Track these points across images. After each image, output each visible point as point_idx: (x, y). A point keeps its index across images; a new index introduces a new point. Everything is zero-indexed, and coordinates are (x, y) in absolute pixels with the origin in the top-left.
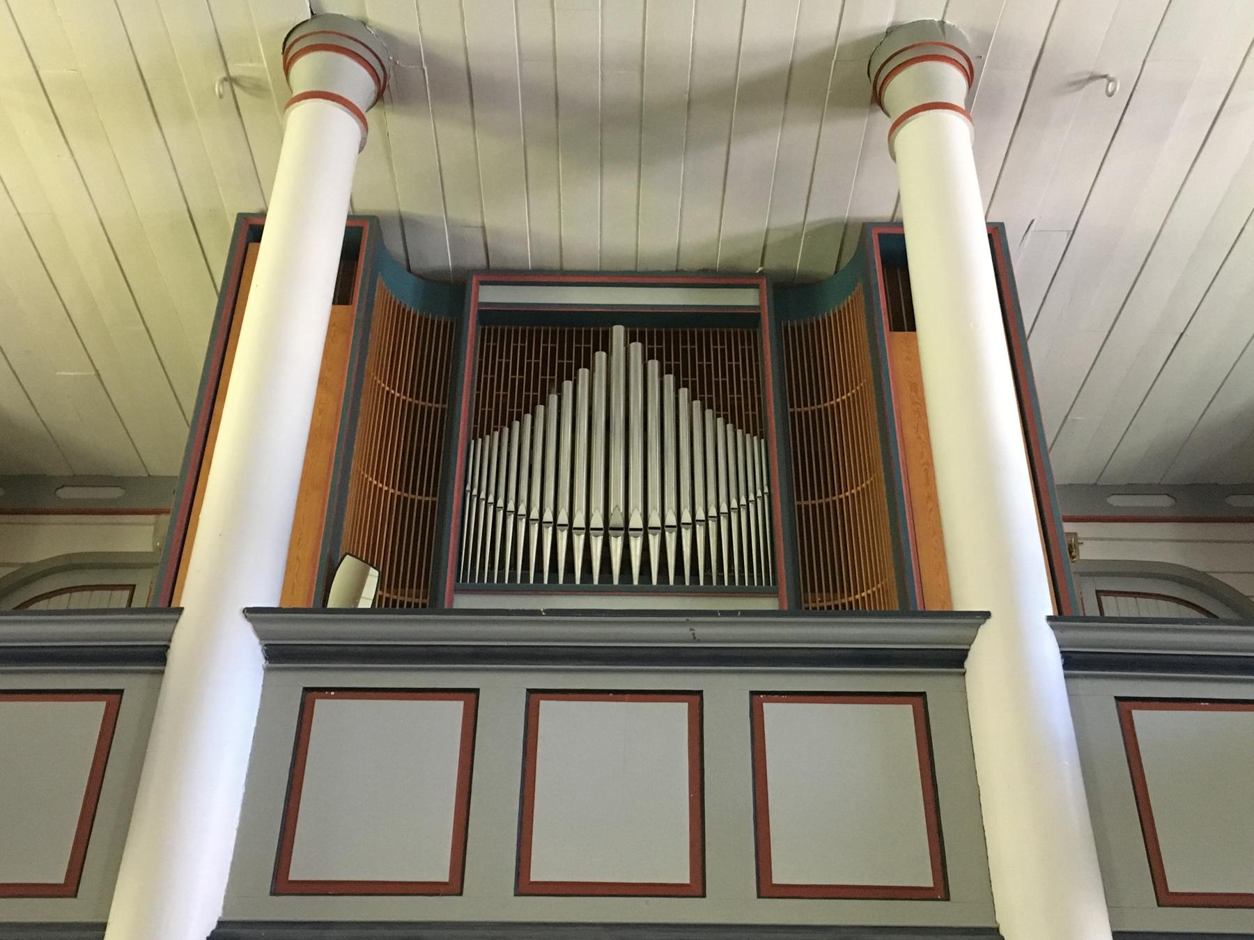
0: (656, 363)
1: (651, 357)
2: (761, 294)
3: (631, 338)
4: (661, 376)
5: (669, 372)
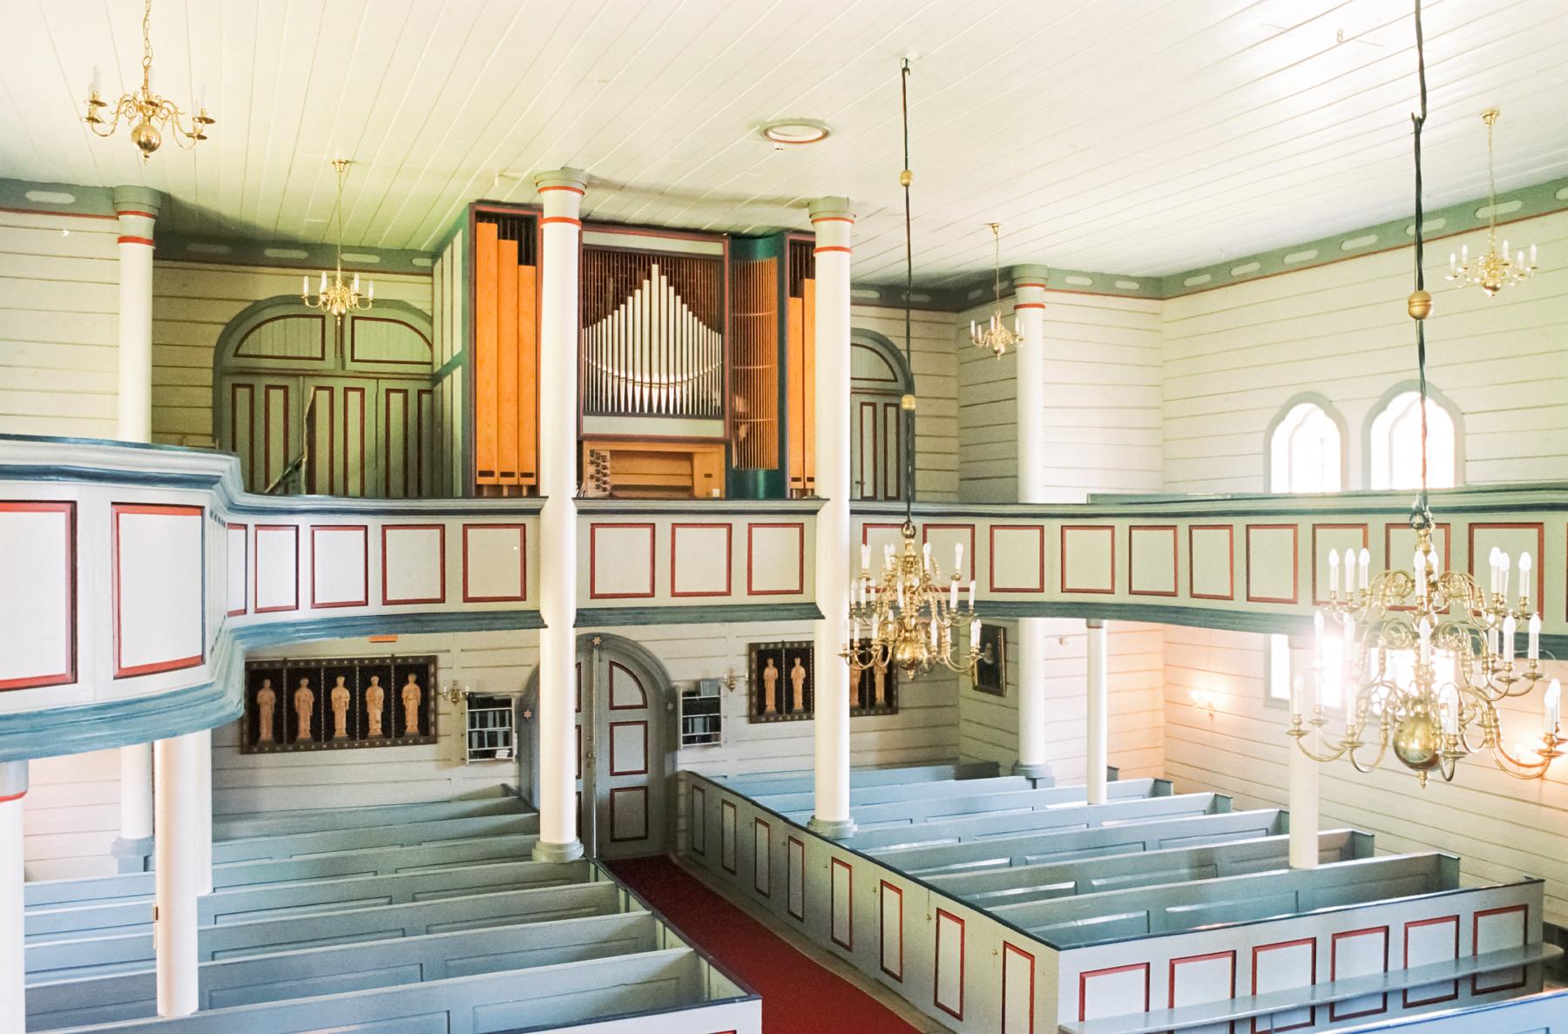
3: (661, 272)
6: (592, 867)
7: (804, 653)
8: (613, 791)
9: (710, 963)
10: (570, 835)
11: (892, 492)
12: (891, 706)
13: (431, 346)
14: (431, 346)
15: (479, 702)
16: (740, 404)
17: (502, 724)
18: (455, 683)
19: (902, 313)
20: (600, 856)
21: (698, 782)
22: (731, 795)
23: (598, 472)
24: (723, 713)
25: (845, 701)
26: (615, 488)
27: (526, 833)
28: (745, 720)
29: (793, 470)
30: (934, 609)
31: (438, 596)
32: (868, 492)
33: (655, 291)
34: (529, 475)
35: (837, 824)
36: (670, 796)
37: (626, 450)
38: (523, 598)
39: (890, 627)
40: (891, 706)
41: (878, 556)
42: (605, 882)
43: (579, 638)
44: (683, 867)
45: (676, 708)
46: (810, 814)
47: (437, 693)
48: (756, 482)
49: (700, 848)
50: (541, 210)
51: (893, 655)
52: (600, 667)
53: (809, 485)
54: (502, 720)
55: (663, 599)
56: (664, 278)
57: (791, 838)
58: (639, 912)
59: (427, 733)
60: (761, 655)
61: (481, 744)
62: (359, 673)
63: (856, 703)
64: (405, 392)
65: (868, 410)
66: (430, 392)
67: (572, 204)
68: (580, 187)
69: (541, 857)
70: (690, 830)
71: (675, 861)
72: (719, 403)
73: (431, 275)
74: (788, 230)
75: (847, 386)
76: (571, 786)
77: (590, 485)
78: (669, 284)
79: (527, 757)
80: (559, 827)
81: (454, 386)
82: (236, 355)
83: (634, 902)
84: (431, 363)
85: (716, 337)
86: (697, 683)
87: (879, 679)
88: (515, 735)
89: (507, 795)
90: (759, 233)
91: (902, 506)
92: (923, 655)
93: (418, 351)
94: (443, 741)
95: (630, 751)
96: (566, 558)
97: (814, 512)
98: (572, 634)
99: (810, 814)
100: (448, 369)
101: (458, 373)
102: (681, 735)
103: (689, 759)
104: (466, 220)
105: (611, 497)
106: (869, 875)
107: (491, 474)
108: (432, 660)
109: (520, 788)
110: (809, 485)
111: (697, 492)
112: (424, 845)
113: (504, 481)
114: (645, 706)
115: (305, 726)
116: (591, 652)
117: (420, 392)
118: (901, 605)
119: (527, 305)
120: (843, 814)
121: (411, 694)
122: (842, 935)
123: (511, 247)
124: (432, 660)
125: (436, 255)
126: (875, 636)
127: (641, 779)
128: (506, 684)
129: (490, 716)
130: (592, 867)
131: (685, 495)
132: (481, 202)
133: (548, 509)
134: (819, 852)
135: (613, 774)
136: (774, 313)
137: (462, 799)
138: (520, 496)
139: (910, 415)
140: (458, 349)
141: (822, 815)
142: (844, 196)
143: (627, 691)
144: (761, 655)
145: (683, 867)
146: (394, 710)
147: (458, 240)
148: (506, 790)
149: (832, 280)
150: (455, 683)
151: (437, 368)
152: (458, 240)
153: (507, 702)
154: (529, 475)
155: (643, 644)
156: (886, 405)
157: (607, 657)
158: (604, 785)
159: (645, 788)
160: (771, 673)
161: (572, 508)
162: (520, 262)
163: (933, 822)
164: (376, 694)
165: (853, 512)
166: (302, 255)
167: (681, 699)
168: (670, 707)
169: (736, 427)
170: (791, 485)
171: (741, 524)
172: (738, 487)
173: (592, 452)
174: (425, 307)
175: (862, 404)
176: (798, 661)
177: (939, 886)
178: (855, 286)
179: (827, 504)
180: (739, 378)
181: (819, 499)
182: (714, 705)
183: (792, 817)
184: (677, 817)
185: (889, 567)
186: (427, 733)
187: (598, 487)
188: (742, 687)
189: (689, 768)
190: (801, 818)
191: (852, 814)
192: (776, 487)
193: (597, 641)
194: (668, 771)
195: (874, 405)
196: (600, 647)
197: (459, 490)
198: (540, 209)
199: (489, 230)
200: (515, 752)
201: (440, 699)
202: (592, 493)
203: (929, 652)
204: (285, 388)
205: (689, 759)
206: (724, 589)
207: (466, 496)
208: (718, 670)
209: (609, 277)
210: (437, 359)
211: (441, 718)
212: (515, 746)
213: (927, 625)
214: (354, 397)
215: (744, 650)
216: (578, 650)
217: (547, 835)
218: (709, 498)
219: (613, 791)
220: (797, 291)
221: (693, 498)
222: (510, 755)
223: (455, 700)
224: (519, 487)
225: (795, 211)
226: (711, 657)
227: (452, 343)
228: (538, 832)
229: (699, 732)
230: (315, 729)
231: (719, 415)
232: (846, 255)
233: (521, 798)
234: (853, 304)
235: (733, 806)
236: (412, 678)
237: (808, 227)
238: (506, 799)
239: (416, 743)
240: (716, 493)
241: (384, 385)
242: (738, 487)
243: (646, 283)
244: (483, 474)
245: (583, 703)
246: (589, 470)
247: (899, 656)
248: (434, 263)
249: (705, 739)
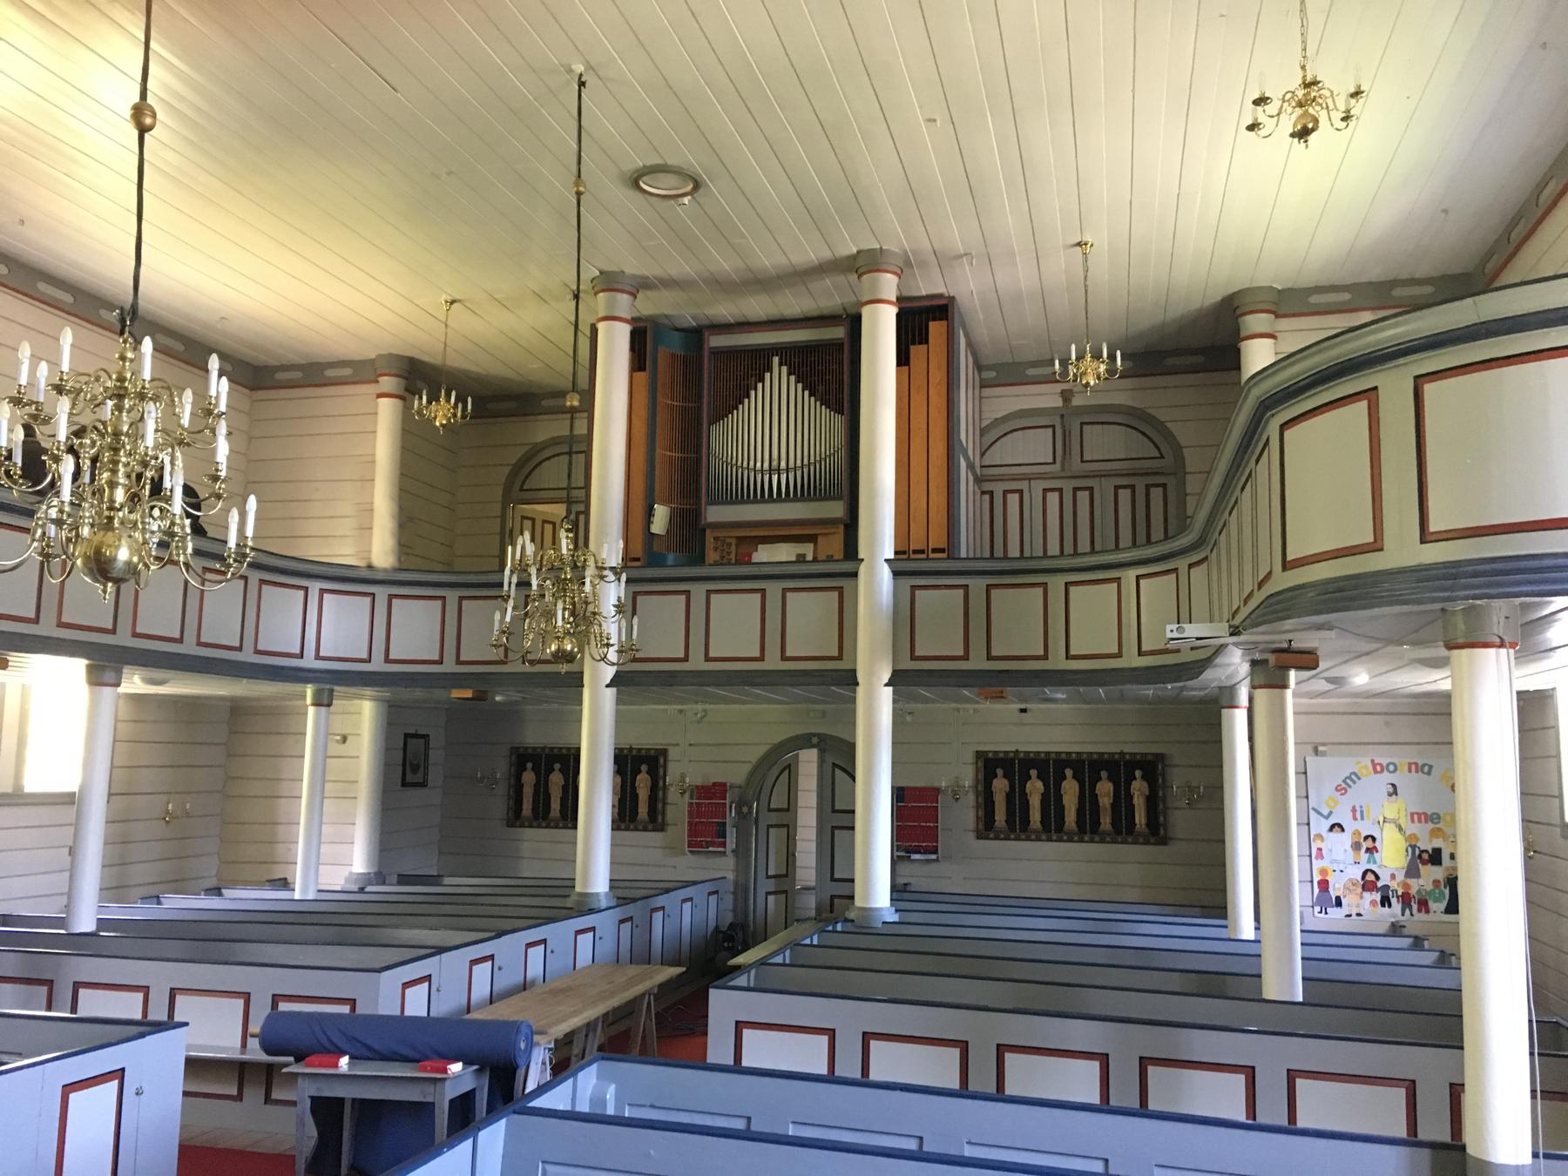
8: (833, 897)
28: (972, 835)
56: (784, 369)
62: (1088, 768)
64: (1060, 490)
78: (797, 382)
82: (521, 490)
94: (670, 829)
115: (1035, 816)
121: (1139, 788)
144: (990, 764)
156: (1076, 489)
160: (1000, 785)
164: (1105, 789)
166: (513, 405)
195: (1132, 488)
204: (1091, 489)
211: (669, 807)
214: (1013, 499)
215: (970, 758)
230: (1010, 821)
236: (644, 768)
241: (1038, 486)
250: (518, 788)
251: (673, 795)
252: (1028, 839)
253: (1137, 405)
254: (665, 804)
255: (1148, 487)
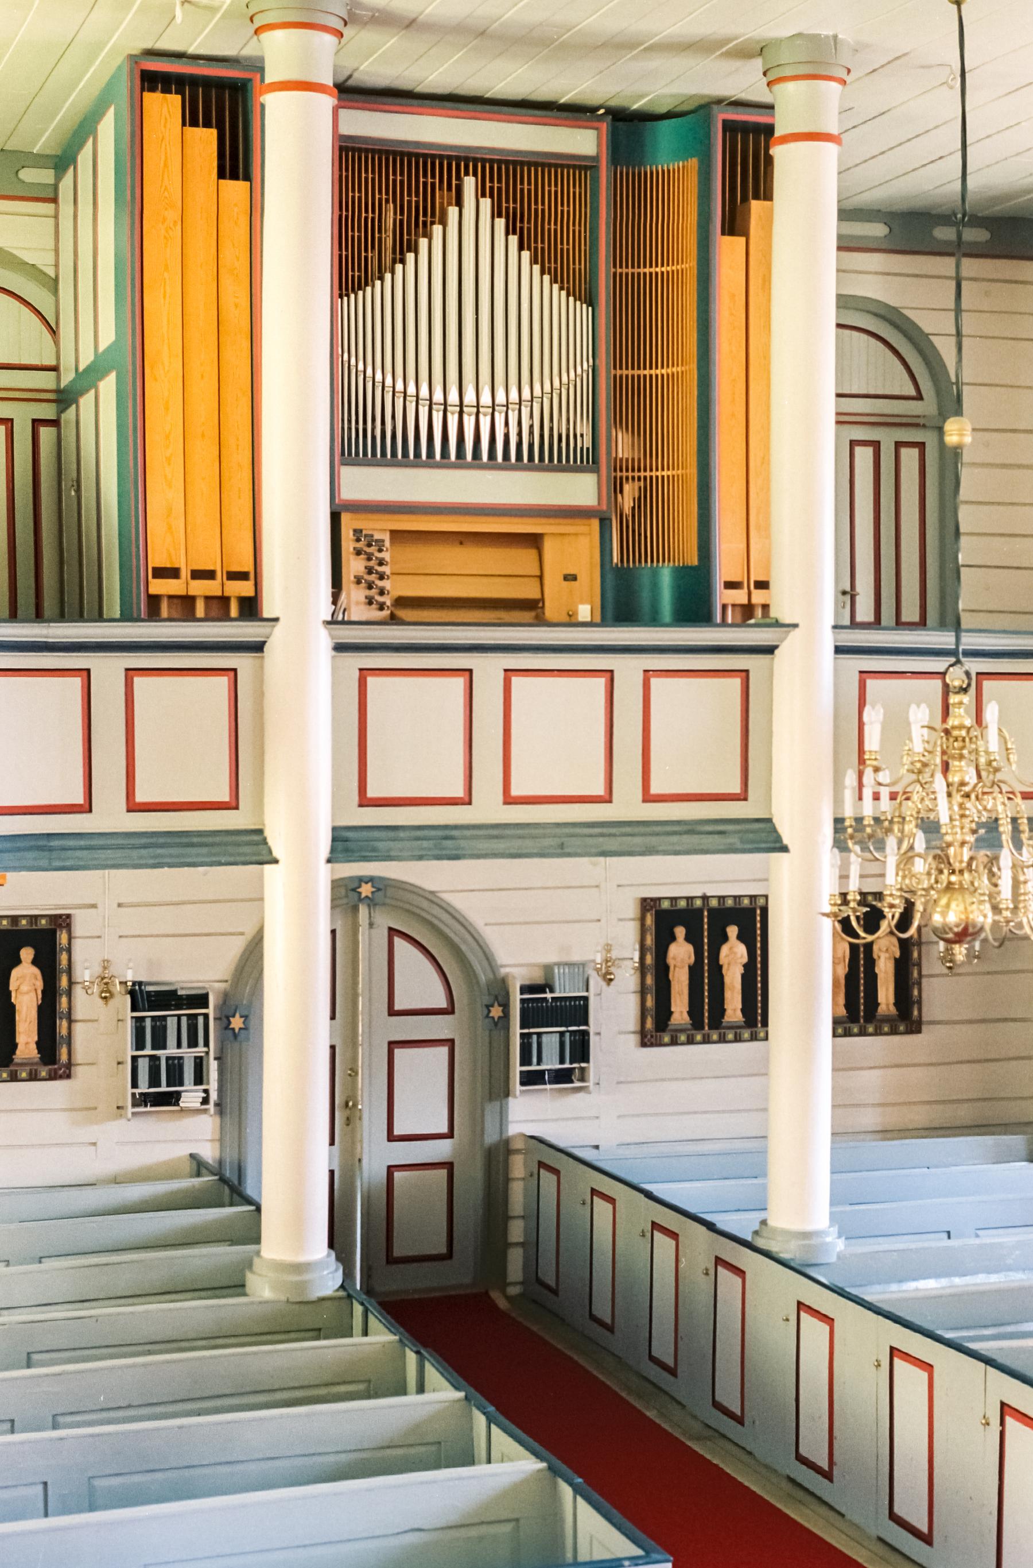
0: (488, 200)
1: (484, 195)
2: (599, 138)
3: (481, 192)
4: (507, 234)
5: (500, 216)
6: (358, 1309)
7: (749, 919)
9: (577, 1490)
10: (317, 1248)
11: (911, 612)
12: (907, 1017)
13: (54, 332)
14: (54, 332)
15: (145, 998)
16: (624, 446)
17: (193, 1043)
18: (106, 964)
19: (946, 265)
20: (368, 1290)
21: (549, 1157)
22: (608, 1181)
23: (370, 571)
24: (592, 1029)
25: (826, 1005)
26: (402, 602)
27: (233, 1242)
28: (634, 1039)
29: (726, 565)
30: (1005, 828)
31: (79, 799)
32: (865, 612)
33: (471, 231)
34: (243, 576)
35: (806, 1235)
36: (490, 1179)
37: (420, 530)
38: (232, 805)
39: (920, 866)
40: (907, 1017)
41: (897, 727)
42: (382, 1336)
43: (336, 885)
44: (496, 1302)
45: (506, 1015)
46: (761, 1215)
47: (71, 983)
48: (655, 586)
49: (551, 1282)
50: (262, 70)
51: (926, 914)
52: (371, 941)
53: (759, 597)
54: (189, 1038)
55: (488, 808)
56: (486, 203)
57: (719, 1261)
58: (442, 1393)
59: (53, 1058)
60: (663, 920)
61: (154, 1081)
63: (842, 1012)
65: (864, 456)
66: (55, 423)
67: (321, 56)
68: (336, 24)
69: (263, 1289)
70: (532, 1246)
71: (502, 1304)
72: (588, 442)
73: (54, 200)
74: (719, 101)
75: (829, 407)
76: (321, 1159)
77: (354, 596)
79: (235, 1106)
80: (295, 1241)
81: (99, 416)
83: (432, 1374)
84: (55, 369)
85: (583, 311)
86: (548, 969)
87: (885, 969)
88: (213, 1066)
89: (198, 1174)
90: (663, 109)
91: (945, 639)
92: (983, 916)
93: (35, 347)
94: (79, 1071)
95: (423, 1095)
96: (309, 728)
97: (769, 650)
98: (323, 875)
99: (761, 1215)
100: (88, 378)
101: (108, 386)
102: (517, 1069)
103: (532, 1114)
104: (123, 89)
105: (394, 620)
106: (864, 1338)
107: (173, 573)
108: (62, 922)
109: (221, 1162)
110: (759, 597)
111: (551, 611)
112: (47, 1264)
113: (200, 588)
114: (450, 1011)
116: (355, 909)
117: (36, 423)
118: (944, 819)
119: (235, 255)
120: (819, 1217)
122: (816, 1449)
123: (205, 140)
124: (62, 922)
125: (63, 161)
126: (892, 881)
127: (442, 1150)
128: (199, 967)
129: (171, 1024)
130: (358, 1309)
131: (528, 616)
132: (150, 53)
133: (278, 640)
134: (773, 1291)
135: (391, 1137)
136: (690, 265)
137: (116, 1180)
138: (225, 617)
139: (956, 452)
140: (108, 336)
141: (783, 1217)
142: (826, 31)
143: (419, 983)
144: (663, 920)
145: (496, 1302)
146: (707, 978)
147: (107, 129)
148: (198, 1165)
149: (806, 195)
150: (106, 964)
151: (67, 378)
152: (107, 129)
153: (201, 1000)
154: (243, 576)
155: (447, 897)
157: (385, 920)
158: (377, 1156)
159: (449, 1166)
161: (323, 640)
162: (221, 175)
163: (988, 1238)
165: (839, 650)
167: (516, 998)
168: (496, 1012)
169: (617, 487)
170: (723, 597)
171: (629, 670)
172: (623, 604)
173: (358, 532)
174: (43, 261)
175: (853, 444)
176: (733, 931)
177: (1001, 1360)
178: (846, 214)
179: (795, 634)
180: (627, 394)
181: (777, 624)
182: (576, 1011)
183: (723, 1222)
184: (507, 1218)
185: (918, 747)
186: (53, 1058)
187: (370, 601)
188: (627, 978)
189: (531, 1130)
190: (740, 1224)
191: (833, 1218)
192: (694, 604)
193: (366, 890)
194: (491, 1137)
196: (371, 902)
197: (113, 605)
198: (258, 66)
199: (165, 109)
200: (214, 1096)
201: (78, 992)
202: (358, 612)
203: (996, 909)
205: (532, 1114)
206: (600, 790)
207: (127, 616)
208: (587, 949)
209: (386, 201)
210: (67, 362)
211: (78, 1029)
212: (213, 1086)
213: (994, 859)
215: (632, 910)
216: (335, 904)
217: (275, 1245)
218: (572, 623)
219: (391, 1169)
220: (735, 224)
221: (541, 621)
222: (205, 1101)
223: (107, 996)
224: (224, 600)
225: (738, 63)
226: (568, 922)
227: (96, 327)
228: (257, 1240)
229: (550, 1063)
230: (695, 1010)
231: (589, 462)
232: (831, 147)
233: (223, 1180)
234: (840, 248)
235: (611, 1200)
237: (760, 94)
238: (197, 1181)
239: (33, 1077)
240: (584, 612)
242: (623, 604)
243: (453, 211)
244: (161, 573)
245: (341, 1002)
246: (353, 566)
247: (937, 919)
248: (58, 178)
249: (562, 1077)
250: (663, 970)
251: (84, 1004)
252: (722, 1040)
253: (893, 302)
254: (70, 1021)
255: (898, 445)
